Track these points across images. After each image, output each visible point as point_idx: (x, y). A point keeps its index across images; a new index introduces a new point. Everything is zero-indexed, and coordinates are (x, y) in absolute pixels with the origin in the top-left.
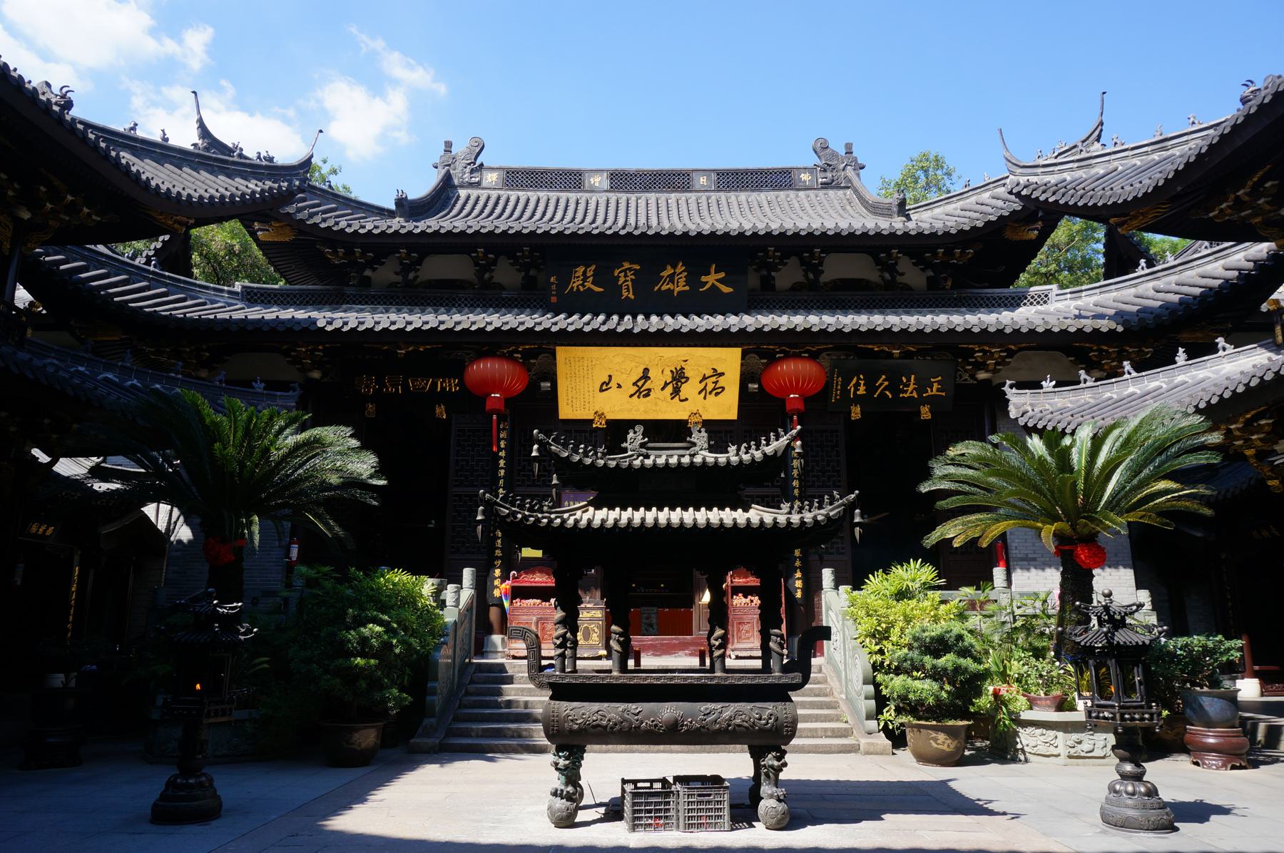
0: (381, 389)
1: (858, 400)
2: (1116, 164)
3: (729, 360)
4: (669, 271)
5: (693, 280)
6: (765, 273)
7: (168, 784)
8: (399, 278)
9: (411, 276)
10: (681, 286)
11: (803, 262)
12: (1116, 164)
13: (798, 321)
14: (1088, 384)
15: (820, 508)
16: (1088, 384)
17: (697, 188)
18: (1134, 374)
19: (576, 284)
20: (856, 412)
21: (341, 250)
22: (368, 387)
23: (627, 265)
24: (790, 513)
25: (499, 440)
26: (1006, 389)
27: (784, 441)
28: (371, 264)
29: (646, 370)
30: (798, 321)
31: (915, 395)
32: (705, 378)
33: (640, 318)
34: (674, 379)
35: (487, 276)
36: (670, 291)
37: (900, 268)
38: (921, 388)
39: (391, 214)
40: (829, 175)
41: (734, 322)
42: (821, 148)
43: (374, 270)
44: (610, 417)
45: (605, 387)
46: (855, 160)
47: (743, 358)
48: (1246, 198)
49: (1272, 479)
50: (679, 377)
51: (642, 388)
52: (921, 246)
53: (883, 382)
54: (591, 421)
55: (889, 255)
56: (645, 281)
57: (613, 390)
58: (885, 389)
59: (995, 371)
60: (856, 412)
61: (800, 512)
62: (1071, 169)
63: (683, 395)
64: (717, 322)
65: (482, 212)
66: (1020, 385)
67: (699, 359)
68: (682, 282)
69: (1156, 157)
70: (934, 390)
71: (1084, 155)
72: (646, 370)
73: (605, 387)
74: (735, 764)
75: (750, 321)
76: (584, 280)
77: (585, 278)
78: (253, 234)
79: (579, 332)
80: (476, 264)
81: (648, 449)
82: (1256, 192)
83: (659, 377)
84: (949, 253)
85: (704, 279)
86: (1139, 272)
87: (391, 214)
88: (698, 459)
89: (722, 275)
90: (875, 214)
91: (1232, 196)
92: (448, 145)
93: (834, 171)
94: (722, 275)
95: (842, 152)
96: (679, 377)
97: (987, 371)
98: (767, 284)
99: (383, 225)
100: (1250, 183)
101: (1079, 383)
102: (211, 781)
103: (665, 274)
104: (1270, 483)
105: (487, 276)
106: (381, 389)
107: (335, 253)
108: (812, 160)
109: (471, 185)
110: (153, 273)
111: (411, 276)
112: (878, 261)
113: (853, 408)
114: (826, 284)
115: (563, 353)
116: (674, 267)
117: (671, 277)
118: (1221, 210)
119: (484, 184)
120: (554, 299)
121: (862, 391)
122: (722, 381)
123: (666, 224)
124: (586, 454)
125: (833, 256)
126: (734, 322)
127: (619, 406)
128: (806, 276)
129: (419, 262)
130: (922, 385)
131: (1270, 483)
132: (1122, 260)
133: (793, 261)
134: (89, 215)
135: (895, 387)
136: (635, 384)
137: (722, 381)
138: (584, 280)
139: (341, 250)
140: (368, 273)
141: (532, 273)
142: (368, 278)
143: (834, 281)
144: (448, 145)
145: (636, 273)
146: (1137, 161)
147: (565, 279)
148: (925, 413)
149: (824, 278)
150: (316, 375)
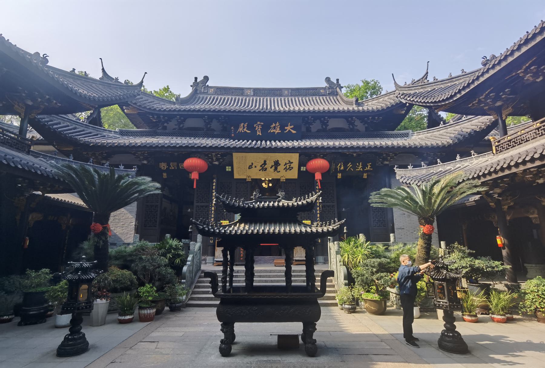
0: (169, 168)
1: (341, 171)
2: (434, 87)
3: (295, 158)
4: (274, 125)
5: (282, 128)
6: (307, 126)
7: (65, 338)
8: (177, 127)
9: (181, 126)
10: (278, 131)
11: (321, 121)
12: (434, 87)
13: (319, 143)
14: (425, 167)
15: (330, 225)
16: (425, 167)
17: (285, 95)
18: (441, 164)
19: (240, 129)
20: (339, 176)
21: (155, 116)
22: (163, 166)
23: (259, 123)
24: (317, 226)
25: (213, 186)
26: (395, 168)
27: (315, 197)
28: (166, 121)
29: (265, 161)
30: (319, 143)
31: (361, 169)
32: (286, 164)
33: (263, 142)
34: (275, 164)
35: (209, 126)
36: (274, 132)
37: (356, 124)
38: (364, 167)
39: (174, 103)
40: (331, 90)
41: (296, 144)
42: (328, 80)
43: (168, 123)
44: (252, 178)
45: (250, 167)
46: (340, 85)
47: (300, 156)
48: (483, 100)
49: (491, 202)
50: (277, 164)
51: (263, 168)
52: (364, 116)
53: (350, 165)
54: (246, 179)
55: (352, 119)
56: (266, 128)
57: (254, 168)
58: (351, 167)
59: (390, 161)
60: (339, 176)
61: (321, 226)
62: (418, 89)
63: (279, 169)
64: (290, 144)
65: (208, 103)
66: (400, 167)
67: (283, 158)
68: (278, 129)
69: (449, 84)
70: (369, 168)
71: (423, 84)
72: (265, 161)
73: (250, 167)
74: (295, 328)
75: (302, 144)
76: (244, 128)
77: (244, 128)
78: (123, 110)
79: (240, 148)
80: (205, 122)
81: (261, 199)
82: (486, 97)
83: (270, 163)
84: (373, 118)
85: (286, 128)
86: (441, 126)
87: (174, 103)
88: (281, 204)
89: (292, 126)
90: (347, 104)
91: (477, 99)
92: (196, 78)
93: (332, 89)
94: (292, 126)
95: (335, 82)
96: (277, 164)
97: (387, 161)
98: (308, 130)
99: (173, 107)
100: (485, 94)
101: (421, 166)
102: (84, 335)
103: (272, 126)
104: (491, 204)
105: (209, 126)
106: (169, 168)
107: (153, 117)
108: (325, 85)
109: (204, 93)
110: (86, 125)
111: (181, 126)
112: (348, 121)
113: (338, 174)
114: (329, 129)
115: (235, 155)
116: (276, 124)
117: (274, 128)
118: (473, 104)
119: (209, 93)
120: (233, 135)
121: (342, 168)
122: (292, 165)
123: (277, 109)
124: (236, 201)
125: (332, 119)
126: (296, 144)
127: (255, 174)
128: (322, 127)
129: (184, 120)
130: (364, 166)
131: (491, 204)
132: (434, 122)
133: (318, 121)
134: (56, 103)
135: (354, 167)
136: (261, 166)
137: (292, 165)
138: (244, 128)
139: (155, 116)
140: (165, 124)
141: (225, 125)
142: (166, 126)
143: (332, 129)
144: (196, 78)
145: (262, 126)
146: (442, 86)
147: (237, 127)
148: (365, 176)
149: (329, 128)
150: (145, 162)
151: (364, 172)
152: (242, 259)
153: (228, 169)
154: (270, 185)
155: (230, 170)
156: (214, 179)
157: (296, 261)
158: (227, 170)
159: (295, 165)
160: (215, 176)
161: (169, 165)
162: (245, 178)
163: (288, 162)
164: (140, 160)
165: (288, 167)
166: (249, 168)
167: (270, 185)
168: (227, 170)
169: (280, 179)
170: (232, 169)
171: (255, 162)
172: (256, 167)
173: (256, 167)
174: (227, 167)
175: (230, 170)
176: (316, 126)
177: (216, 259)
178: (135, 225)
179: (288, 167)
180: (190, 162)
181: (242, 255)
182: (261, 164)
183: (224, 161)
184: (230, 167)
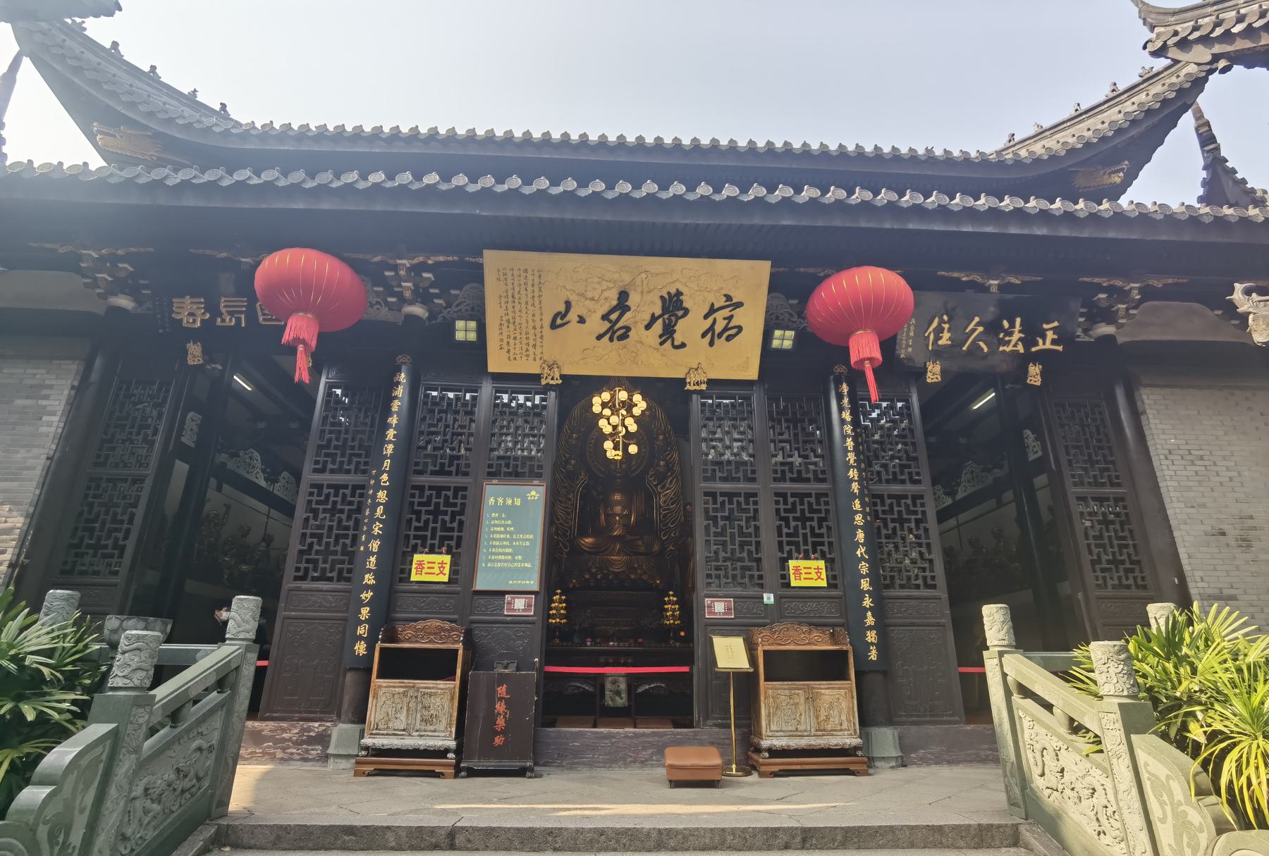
0: (213, 319)
1: (938, 354)
3: (749, 280)
29: (623, 295)
31: (1021, 348)
32: (712, 310)
34: (665, 310)
38: (1028, 341)
44: (568, 371)
50: (673, 306)
70: (1046, 344)
72: (623, 295)
83: (645, 305)
106: (213, 319)
115: (492, 260)
122: (740, 317)
136: (605, 317)
137: (740, 317)
151: (1029, 358)
152: (498, 740)
153: (464, 331)
154: (633, 449)
155: (472, 336)
156: (398, 370)
157: (775, 753)
158: (460, 336)
159: (752, 319)
160: (400, 359)
161: (212, 308)
162: (537, 371)
163: (721, 302)
164: (104, 296)
165: (718, 328)
166: (554, 326)
167: (633, 449)
168: (460, 336)
169: (682, 382)
170: (481, 330)
171: (582, 295)
172: (582, 320)
173: (582, 320)
174: (460, 324)
175: (472, 336)
176: (460, 839)
177: (368, 741)
178: (12, 566)
179: (718, 328)
180: (277, 264)
181: (501, 722)
182: (605, 309)
183: (449, 305)
184: (473, 324)
